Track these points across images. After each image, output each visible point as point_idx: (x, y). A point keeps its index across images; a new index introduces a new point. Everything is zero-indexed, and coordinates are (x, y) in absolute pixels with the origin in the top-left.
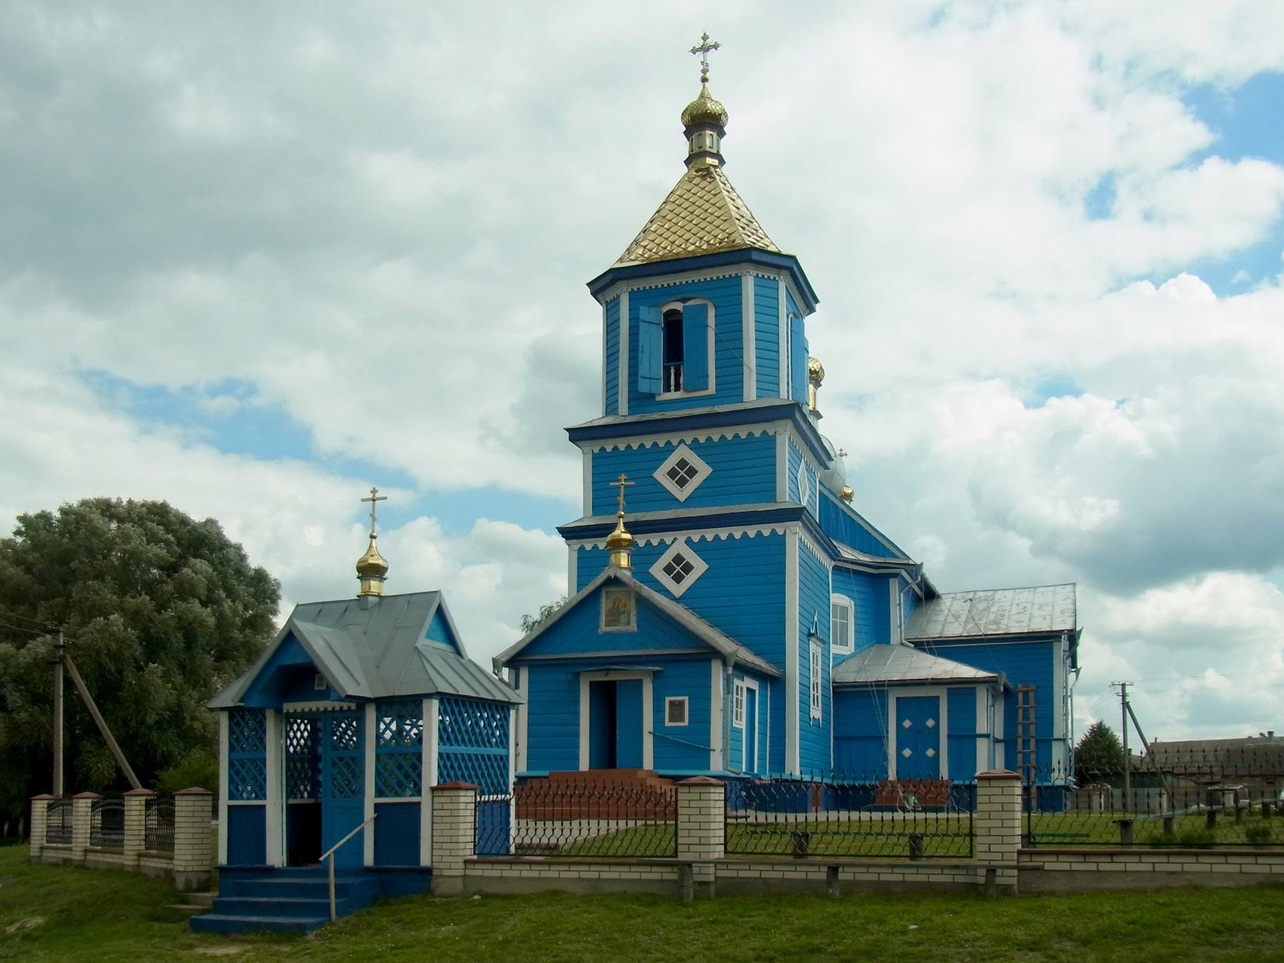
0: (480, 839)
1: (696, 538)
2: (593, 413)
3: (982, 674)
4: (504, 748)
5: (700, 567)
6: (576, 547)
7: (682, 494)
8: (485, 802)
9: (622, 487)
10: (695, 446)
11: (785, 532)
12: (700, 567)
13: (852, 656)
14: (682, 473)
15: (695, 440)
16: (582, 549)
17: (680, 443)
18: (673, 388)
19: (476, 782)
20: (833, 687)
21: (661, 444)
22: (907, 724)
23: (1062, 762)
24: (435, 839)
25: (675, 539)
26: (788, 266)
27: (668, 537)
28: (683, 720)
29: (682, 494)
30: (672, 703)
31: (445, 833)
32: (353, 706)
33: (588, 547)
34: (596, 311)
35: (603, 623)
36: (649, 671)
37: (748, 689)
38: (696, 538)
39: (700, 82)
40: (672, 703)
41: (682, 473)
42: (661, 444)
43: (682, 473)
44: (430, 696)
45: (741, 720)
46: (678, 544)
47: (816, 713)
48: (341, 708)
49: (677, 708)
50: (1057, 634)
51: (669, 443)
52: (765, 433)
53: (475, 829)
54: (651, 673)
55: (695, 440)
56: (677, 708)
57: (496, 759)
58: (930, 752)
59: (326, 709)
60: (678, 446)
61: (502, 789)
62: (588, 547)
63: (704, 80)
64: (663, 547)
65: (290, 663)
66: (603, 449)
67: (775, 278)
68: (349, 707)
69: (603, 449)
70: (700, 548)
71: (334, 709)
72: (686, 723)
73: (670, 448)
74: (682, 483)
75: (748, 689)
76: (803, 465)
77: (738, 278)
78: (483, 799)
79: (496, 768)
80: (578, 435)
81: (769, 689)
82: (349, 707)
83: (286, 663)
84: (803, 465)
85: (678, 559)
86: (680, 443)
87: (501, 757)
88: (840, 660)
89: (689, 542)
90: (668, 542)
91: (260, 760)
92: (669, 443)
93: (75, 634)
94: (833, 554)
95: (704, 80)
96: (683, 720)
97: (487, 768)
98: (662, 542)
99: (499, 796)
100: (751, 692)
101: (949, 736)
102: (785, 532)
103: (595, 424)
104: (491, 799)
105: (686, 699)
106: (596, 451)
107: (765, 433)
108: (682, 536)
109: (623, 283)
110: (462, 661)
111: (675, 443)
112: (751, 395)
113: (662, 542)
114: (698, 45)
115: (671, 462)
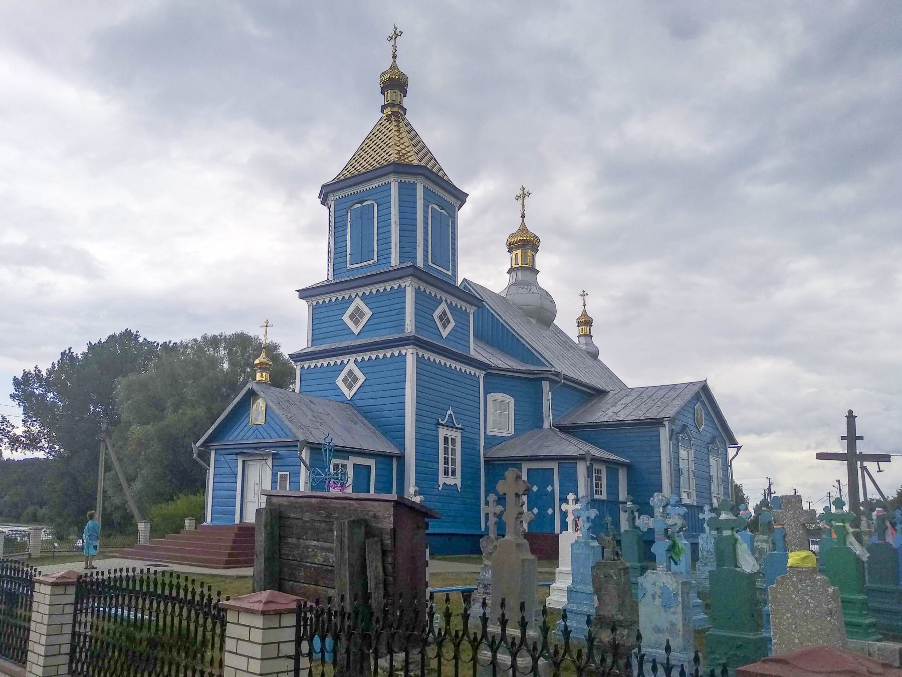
10: (363, 298)
13: (512, 437)
14: (357, 316)
17: (356, 296)
27: (345, 359)
49: (283, 478)
51: (350, 296)
60: (355, 298)
66: (318, 303)
73: (351, 300)
108: (352, 358)
112: (395, 261)
113: (342, 362)
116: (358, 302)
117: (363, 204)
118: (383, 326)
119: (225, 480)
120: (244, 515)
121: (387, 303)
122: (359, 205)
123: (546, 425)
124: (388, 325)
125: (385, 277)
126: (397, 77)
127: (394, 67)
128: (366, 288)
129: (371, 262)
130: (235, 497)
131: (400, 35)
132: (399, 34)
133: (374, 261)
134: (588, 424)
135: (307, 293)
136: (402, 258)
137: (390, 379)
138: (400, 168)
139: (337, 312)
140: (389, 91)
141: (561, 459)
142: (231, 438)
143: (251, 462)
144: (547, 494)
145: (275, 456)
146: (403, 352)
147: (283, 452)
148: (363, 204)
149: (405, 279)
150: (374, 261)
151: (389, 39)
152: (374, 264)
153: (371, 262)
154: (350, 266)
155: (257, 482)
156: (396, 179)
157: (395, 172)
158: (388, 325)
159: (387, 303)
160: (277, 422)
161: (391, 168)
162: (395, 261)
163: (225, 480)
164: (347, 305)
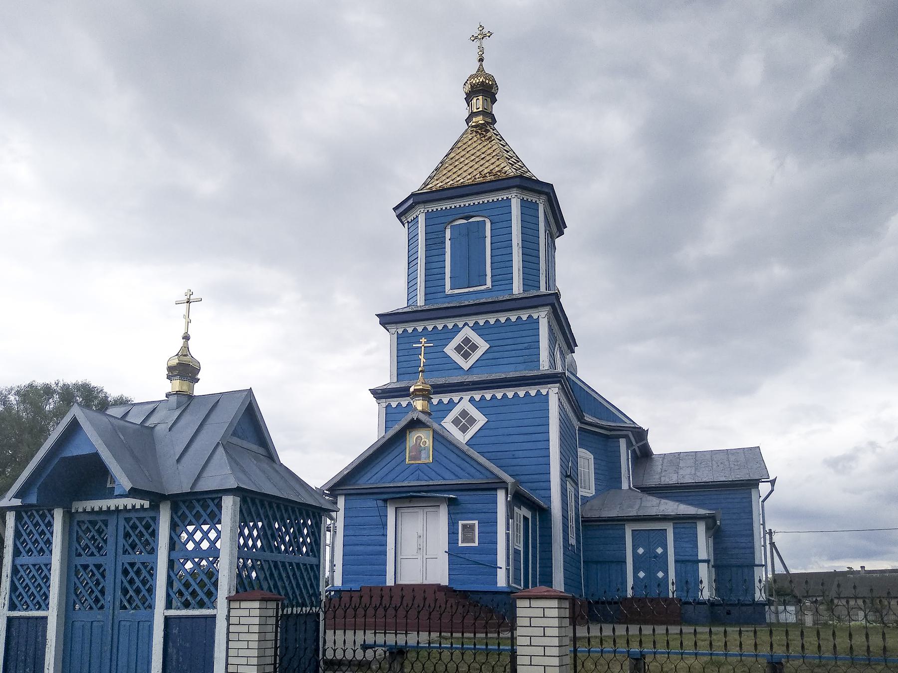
0: (281, 660)
1: (477, 397)
2: (399, 303)
3: (702, 512)
4: (315, 556)
5: (481, 420)
6: (384, 405)
7: (466, 365)
8: (298, 615)
9: (423, 347)
10: (476, 328)
11: (548, 392)
12: (481, 420)
13: (593, 497)
14: (468, 347)
15: (476, 323)
16: (389, 406)
17: (464, 325)
18: (381, 548)
19: (283, 593)
20: (582, 521)
21: (450, 326)
22: (659, 551)
23: (9, 576)
24: (231, 661)
25: (462, 398)
26: (547, 191)
27: (456, 397)
28: (474, 542)
29: (466, 365)
30: (464, 526)
31: (241, 653)
32: (147, 504)
33: (394, 405)
34: (401, 232)
35: (407, 460)
36: (445, 497)
37: (524, 516)
38: (477, 397)
39: (477, 62)
40: (464, 526)
41: (468, 347)
42: (450, 326)
43: (466, 348)
44: (227, 491)
45: (520, 544)
46: (464, 403)
47: (572, 541)
48: (134, 507)
49: (468, 529)
50: (755, 482)
51: (456, 325)
52: (530, 317)
53: (276, 648)
54: (447, 499)
55: (476, 323)
56: (468, 529)
57: (306, 569)
58: (660, 575)
59: (117, 508)
60: (463, 327)
61: (297, 602)
62: (394, 405)
63: (481, 60)
64: (452, 404)
65: (75, 454)
66: (405, 331)
67: (536, 201)
68: (142, 506)
69: (405, 331)
70: (480, 405)
71: (125, 507)
72: (476, 544)
73: (456, 330)
74: (466, 356)
75: (524, 516)
76: (557, 346)
77: (508, 200)
78: (285, 612)
79: (292, 578)
80: (387, 320)
81: (538, 518)
82: (142, 506)
83: (76, 452)
84: (557, 346)
85: (464, 414)
86: (464, 325)
87: (311, 566)
88: (586, 500)
89: (472, 400)
90: (456, 400)
91: (46, 565)
92: (456, 325)
93: (637, 659)
94: (580, 418)
95: (481, 60)
96: (474, 542)
97: (310, 579)
98: (451, 401)
99: (314, 609)
100: (526, 519)
101: (676, 561)
102: (548, 392)
103: (400, 311)
104: (295, 612)
105: (476, 522)
106: (400, 331)
107: (530, 317)
108: (467, 396)
109: (422, 206)
110: (275, 465)
111: (460, 325)
112: (517, 288)
113: (451, 401)
114: (476, 33)
115: (457, 340)
116: (467, 332)
117: (469, 221)
118: (506, 361)
119: (364, 532)
120: (398, 575)
121: (510, 335)
122: (464, 221)
123: (625, 486)
124: (512, 360)
125: (489, 307)
126: (490, 83)
127: (481, 70)
128: (480, 317)
129: (483, 288)
130: (384, 553)
131: (489, 37)
132: (488, 35)
133: (486, 286)
134: (673, 485)
135: (388, 319)
136: (526, 285)
137: (526, 422)
138: (500, 184)
139: (439, 343)
140: (480, 98)
141: (677, 519)
142: (360, 482)
143: (406, 510)
144: (656, 556)
145: (452, 502)
146: (544, 392)
147: (463, 497)
148: (469, 221)
149: (539, 308)
150: (486, 286)
151: (472, 39)
152: (488, 291)
153: (483, 288)
154: (451, 291)
155: (420, 533)
156: (519, 195)
157: (518, 187)
158: (512, 360)
159: (510, 335)
160: (453, 460)
161: (517, 182)
162: (517, 288)
163: (364, 532)
164: (450, 335)
